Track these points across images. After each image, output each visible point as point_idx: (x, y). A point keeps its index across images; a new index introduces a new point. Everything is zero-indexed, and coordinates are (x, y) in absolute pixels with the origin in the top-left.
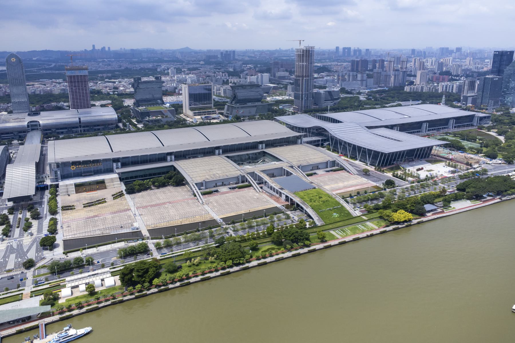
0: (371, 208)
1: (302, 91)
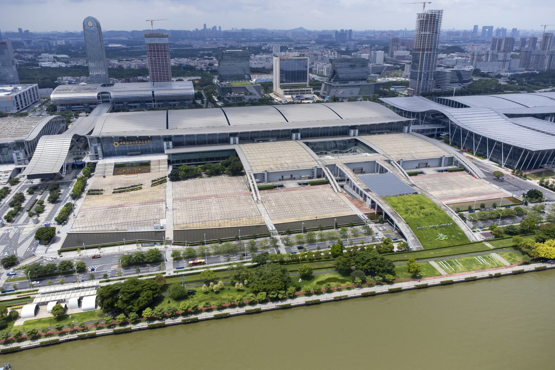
0: (502, 230)
1: (421, 69)
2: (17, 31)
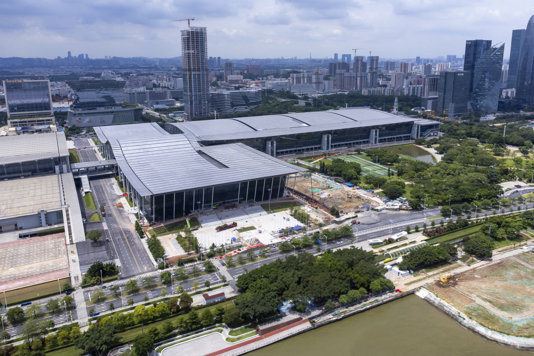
1: (191, 91)
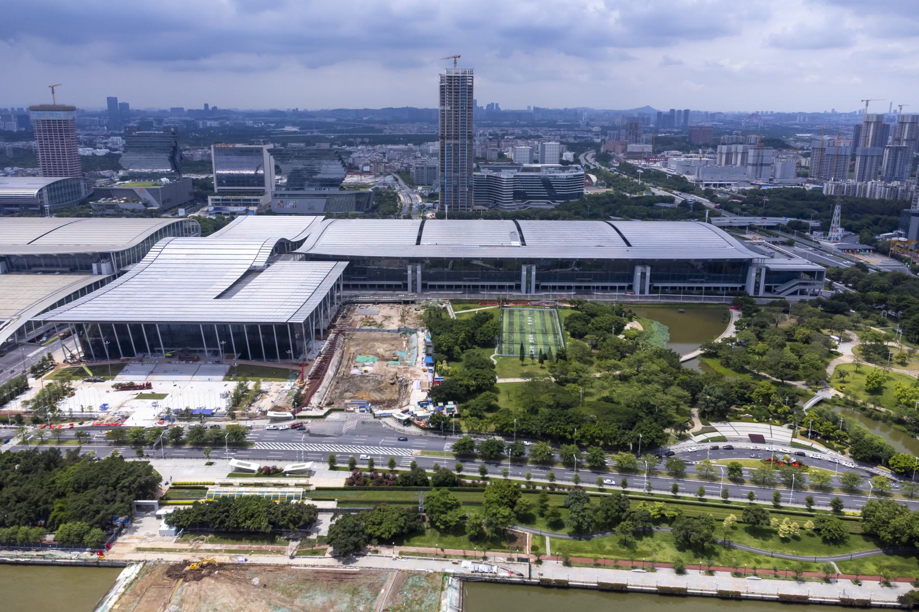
2: (203, 108)
